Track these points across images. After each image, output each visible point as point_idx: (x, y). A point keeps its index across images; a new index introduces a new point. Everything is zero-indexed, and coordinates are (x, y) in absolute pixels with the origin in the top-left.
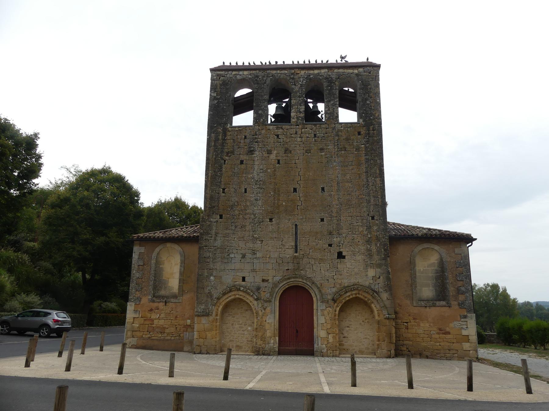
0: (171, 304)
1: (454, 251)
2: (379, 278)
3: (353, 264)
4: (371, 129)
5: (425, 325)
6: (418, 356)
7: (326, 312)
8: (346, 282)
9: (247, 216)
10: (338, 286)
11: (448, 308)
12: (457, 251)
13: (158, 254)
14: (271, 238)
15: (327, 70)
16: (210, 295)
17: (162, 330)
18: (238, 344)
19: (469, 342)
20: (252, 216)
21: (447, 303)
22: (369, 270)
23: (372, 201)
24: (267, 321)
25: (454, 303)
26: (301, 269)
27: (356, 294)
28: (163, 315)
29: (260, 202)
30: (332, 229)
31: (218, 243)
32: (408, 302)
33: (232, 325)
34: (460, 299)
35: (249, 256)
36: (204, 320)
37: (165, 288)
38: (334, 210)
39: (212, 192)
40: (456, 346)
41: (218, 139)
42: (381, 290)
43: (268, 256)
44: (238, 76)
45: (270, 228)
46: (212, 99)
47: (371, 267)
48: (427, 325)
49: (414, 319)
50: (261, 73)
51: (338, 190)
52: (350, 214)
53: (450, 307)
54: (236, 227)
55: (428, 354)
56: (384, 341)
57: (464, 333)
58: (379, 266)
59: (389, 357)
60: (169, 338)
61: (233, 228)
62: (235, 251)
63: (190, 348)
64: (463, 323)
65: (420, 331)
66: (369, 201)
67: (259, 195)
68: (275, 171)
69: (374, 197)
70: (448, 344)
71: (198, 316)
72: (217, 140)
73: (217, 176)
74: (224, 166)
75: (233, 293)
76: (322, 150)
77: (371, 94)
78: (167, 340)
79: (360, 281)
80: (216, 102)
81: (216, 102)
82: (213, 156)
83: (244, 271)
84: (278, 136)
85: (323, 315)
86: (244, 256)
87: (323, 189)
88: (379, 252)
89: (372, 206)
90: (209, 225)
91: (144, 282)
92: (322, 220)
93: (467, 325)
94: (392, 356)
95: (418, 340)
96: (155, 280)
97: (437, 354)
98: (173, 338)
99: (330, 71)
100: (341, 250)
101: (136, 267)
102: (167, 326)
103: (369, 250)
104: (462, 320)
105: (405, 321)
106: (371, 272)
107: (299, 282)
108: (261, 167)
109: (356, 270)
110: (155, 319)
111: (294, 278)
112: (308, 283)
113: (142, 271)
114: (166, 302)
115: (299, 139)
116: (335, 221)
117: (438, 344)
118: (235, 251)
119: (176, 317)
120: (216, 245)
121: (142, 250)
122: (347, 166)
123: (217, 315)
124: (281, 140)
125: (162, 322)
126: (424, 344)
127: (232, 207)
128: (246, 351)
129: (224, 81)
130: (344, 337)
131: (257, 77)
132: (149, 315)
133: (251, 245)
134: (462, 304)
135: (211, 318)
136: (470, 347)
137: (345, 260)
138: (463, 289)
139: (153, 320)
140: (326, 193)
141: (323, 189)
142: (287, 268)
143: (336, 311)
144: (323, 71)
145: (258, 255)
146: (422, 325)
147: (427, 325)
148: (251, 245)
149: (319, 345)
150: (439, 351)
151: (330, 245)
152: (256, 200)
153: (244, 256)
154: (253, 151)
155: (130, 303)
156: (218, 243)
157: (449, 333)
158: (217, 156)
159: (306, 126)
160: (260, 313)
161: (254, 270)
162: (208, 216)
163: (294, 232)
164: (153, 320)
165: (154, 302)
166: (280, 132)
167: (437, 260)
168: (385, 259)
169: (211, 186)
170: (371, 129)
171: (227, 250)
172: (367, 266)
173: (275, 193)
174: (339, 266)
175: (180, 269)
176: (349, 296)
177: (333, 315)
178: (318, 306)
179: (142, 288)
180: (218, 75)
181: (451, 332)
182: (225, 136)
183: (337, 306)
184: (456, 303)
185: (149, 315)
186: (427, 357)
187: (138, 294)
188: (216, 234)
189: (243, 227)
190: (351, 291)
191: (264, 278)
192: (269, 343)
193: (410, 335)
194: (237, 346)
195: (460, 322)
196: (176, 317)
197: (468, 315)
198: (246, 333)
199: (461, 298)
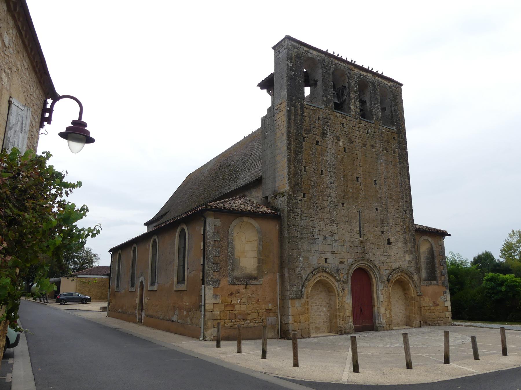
0: (251, 286)
7: (383, 291)
8: (394, 266)
9: (325, 198)
14: (344, 222)
15: (324, 55)
16: (300, 276)
17: (244, 316)
18: (317, 325)
20: (329, 199)
24: (346, 302)
28: (244, 300)
29: (334, 186)
31: (304, 223)
35: (329, 238)
36: (297, 303)
37: (238, 268)
38: (384, 202)
39: (295, 168)
40: (442, 315)
41: (297, 114)
42: (414, 272)
44: (309, 53)
45: (343, 212)
50: (326, 58)
54: (317, 208)
55: (429, 322)
60: (252, 325)
62: (318, 232)
63: (273, 334)
66: (403, 199)
67: (333, 179)
68: (343, 158)
69: (405, 194)
71: (292, 299)
73: (298, 152)
74: (304, 143)
75: (319, 275)
78: (251, 327)
79: (402, 264)
80: (293, 73)
81: (293, 73)
82: (294, 130)
85: (382, 294)
86: (325, 238)
90: (295, 203)
91: (221, 261)
92: (377, 209)
97: (434, 321)
98: (256, 325)
100: (389, 237)
101: (212, 242)
102: (249, 312)
103: (405, 239)
108: (333, 152)
110: (237, 304)
111: (362, 260)
112: (371, 266)
113: (218, 247)
114: (246, 285)
115: (358, 132)
118: (318, 232)
119: (258, 301)
120: (301, 224)
121: (218, 222)
124: (346, 130)
125: (243, 308)
126: (427, 315)
127: (313, 186)
128: (323, 332)
131: (324, 61)
132: (229, 300)
133: (330, 227)
139: (234, 306)
145: (336, 237)
148: (330, 227)
149: (381, 321)
151: (383, 232)
152: (331, 183)
153: (325, 238)
154: (326, 134)
155: (208, 286)
157: (438, 305)
158: (297, 130)
159: (362, 122)
160: (341, 294)
161: (333, 252)
162: (294, 193)
164: (234, 306)
165: (234, 284)
166: (344, 121)
167: (427, 249)
168: (414, 247)
169: (294, 162)
171: (311, 230)
173: (344, 179)
174: (389, 251)
175: (258, 248)
179: (220, 268)
180: (293, 46)
185: (229, 300)
186: (429, 325)
187: (216, 275)
188: (302, 212)
189: (323, 208)
191: (341, 260)
192: (348, 323)
194: (316, 328)
196: (258, 301)
198: (322, 314)
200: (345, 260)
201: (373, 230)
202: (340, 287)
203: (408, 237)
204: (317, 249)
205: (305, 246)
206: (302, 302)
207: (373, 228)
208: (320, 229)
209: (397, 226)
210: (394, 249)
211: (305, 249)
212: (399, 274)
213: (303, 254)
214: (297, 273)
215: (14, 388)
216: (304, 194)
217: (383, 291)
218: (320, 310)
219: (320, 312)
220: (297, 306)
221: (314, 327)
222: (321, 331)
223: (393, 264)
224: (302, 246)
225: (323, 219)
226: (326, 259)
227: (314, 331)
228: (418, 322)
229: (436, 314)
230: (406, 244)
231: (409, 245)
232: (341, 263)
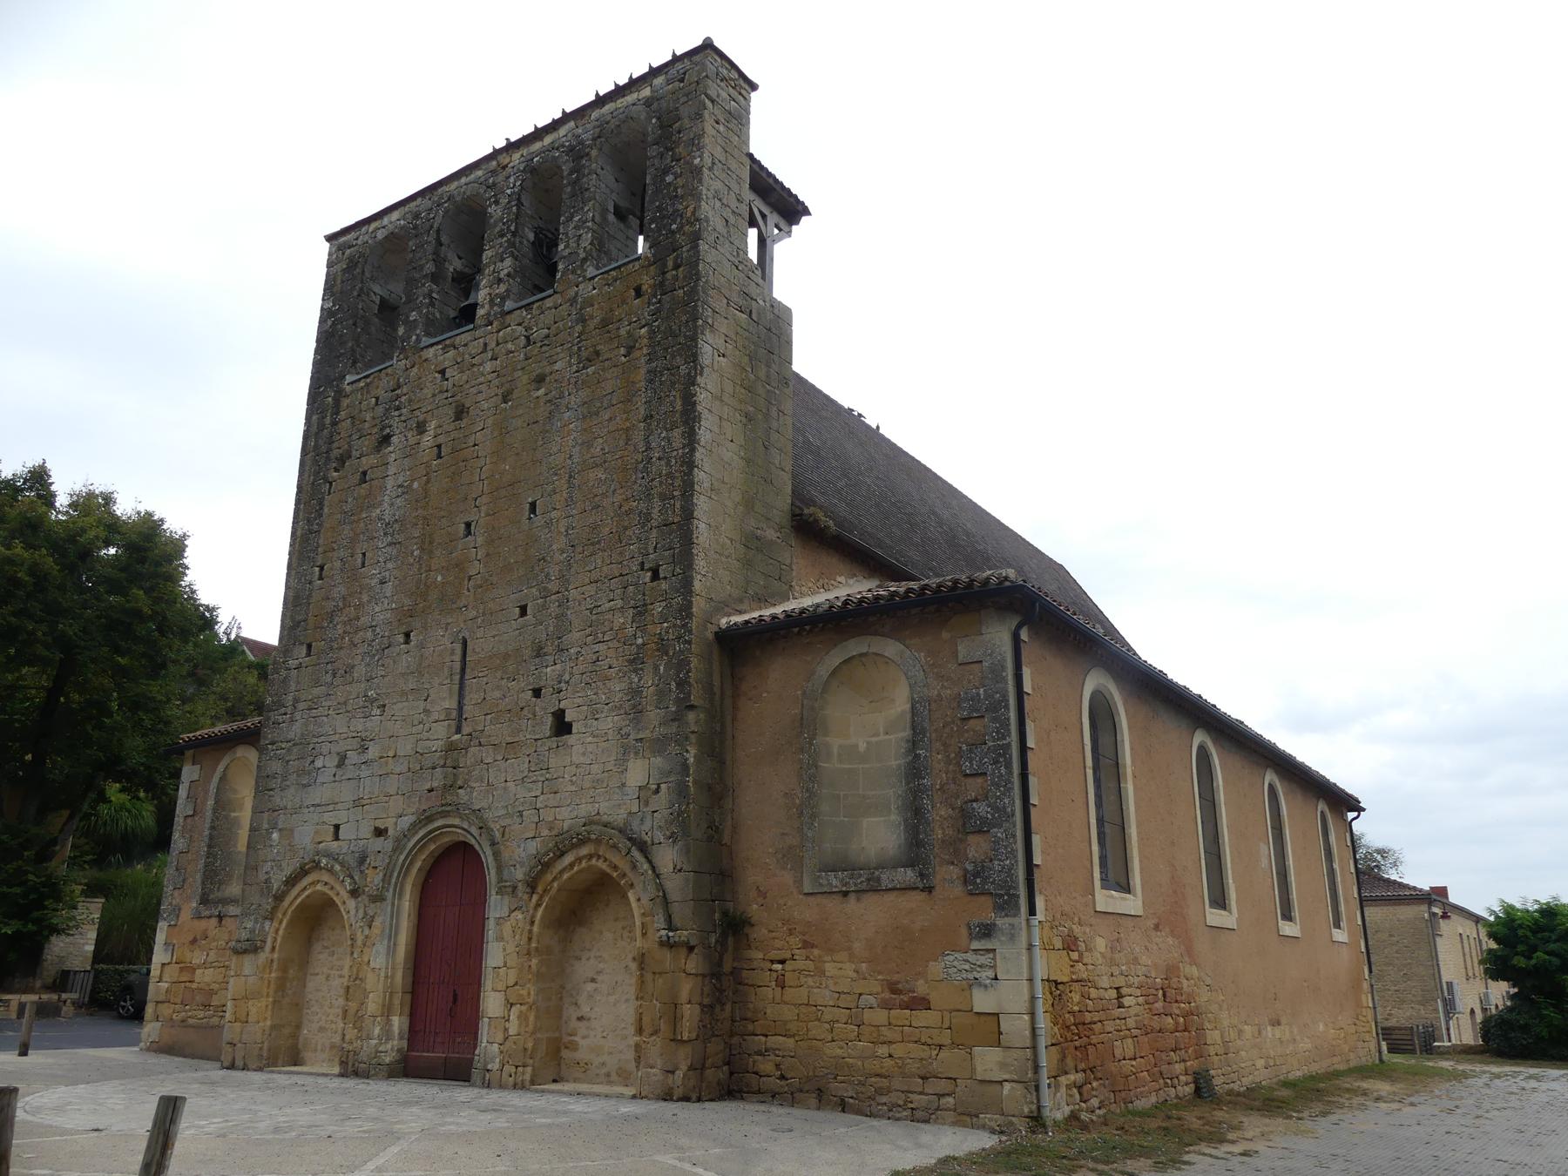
1: (955, 654)
2: (657, 791)
3: (590, 748)
4: (670, 264)
5: (841, 971)
6: (813, 1101)
7: (507, 928)
8: (568, 816)
10: (545, 832)
11: (924, 894)
12: (964, 650)
13: (223, 779)
14: (404, 693)
19: (999, 1045)
21: (922, 875)
22: (630, 764)
23: (655, 513)
24: (372, 964)
25: (947, 875)
26: (460, 783)
27: (590, 857)
30: (544, 636)
31: (295, 731)
32: (787, 878)
33: (327, 978)
34: (972, 853)
35: (353, 757)
38: (554, 571)
40: (948, 1060)
43: (391, 754)
46: (326, 314)
47: (636, 753)
48: (849, 970)
49: (807, 945)
51: (570, 501)
52: (594, 576)
53: (929, 890)
55: (848, 1092)
56: (655, 1033)
57: (983, 1001)
58: (659, 745)
59: (667, 1096)
61: (329, 678)
64: (982, 959)
65: (824, 996)
68: (428, 482)
69: (663, 497)
70: (918, 1051)
72: (321, 427)
76: (540, 380)
77: (680, 150)
79: (604, 807)
83: (339, 806)
84: (443, 372)
87: (533, 506)
88: (661, 694)
89: (654, 533)
92: (523, 611)
93: (994, 967)
94: (678, 1093)
95: (813, 1033)
96: (209, 855)
97: (880, 1091)
99: (580, 123)
104: (975, 945)
105: (774, 955)
106: (637, 773)
107: (458, 828)
109: (595, 768)
110: (199, 967)
114: (220, 917)
116: (554, 608)
117: (882, 1050)
122: (597, 414)
123: (273, 948)
129: (351, 259)
130: (580, 1019)
134: (976, 874)
135: (263, 956)
136: (1003, 1066)
137: (570, 739)
138: (982, 809)
140: (539, 520)
141: (533, 506)
142: (428, 786)
143: (532, 923)
144: (562, 131)
145: (373, 752)
146: (830, 968)
147: (849, 970)
149: (489, 1046)
150: (884, 1083)
151: (537, 693)
156: (295, 731)
157: (923, 1004)
160: (360, 938)
161: (358, 803)
163: (457, 666)
170: (670, 264)
172: (626, 750)
174: (553, 762)
176: (572, 865)
177: (525, 939)
178: (496, 906)
181: (934, 998)
182: (337, 413)
183: (538, 905)
184: (954, 872)
186: (843, 1107)
188: (296, 700)
189: (349, 669)
190: (574, 846)
193: (788, 1013)
195: (971, 957)
197: (999, 922)
199: (976, 847)
200: (389, 823)
201: (497, 694)
203: (649, 680)
204: (317, 801)
207: (498, 687)
208: (332, 738)
209: (602, 647)
212: (584, 851)
214: (262, 877)
215: (81, 1104)
216: (309, 646)
217: (507, 928)
220: (246, 972)
223: (564, 813)
226: (337, 827)
229: (898, 1050)
231: (654, 715)
232: (380, 832)
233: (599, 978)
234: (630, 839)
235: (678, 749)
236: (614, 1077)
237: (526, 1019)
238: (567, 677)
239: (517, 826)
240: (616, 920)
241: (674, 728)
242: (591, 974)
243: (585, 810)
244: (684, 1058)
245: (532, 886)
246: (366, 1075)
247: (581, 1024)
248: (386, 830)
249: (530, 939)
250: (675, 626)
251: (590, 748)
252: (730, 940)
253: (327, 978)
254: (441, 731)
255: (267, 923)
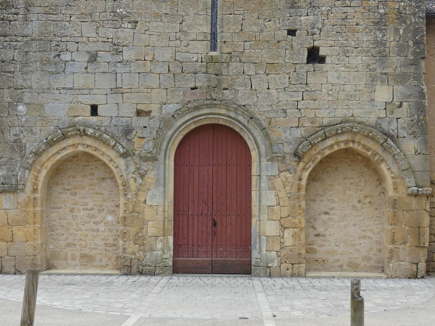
2: (400, 106)
7: (278, 182)
8: (325, 116)
14: (157, 16)
18: (87, 251)
22: (378, 88)
24: (149, 203)
26: (225, 86)
31: (33, 28)
35: (105, 57)
42: (403, 133)
56: (405, 243)
58: (402, 79)
62: (72, 47)
79: (357, 112)
86: (93, 58)
100: (316, 44)
103: (380, 44)
106: (383, 94)
107: (221, 115)
109: (348, 88)
111: (208, 106)
112: (240, 118)
118: (72, 47)
120: (27, 31)
123: (35, 190)
130: (318, 235)
142: (192, 85)
143: (300, 179)
151: (292, 33)
153: (93, 58)
156: (33, 28)
160: (133, 186)
161: (117, 90)
171: (54, 44)
172: (373, 79)
174: (311, 80)
178: (261, 168)
183: (304, 169)
191: (140, 107)
192: (151, 250)
194: (83, 256)
198: (102, 227)
201: (255, 28)
202: (132, 168)
205: (35, 80)
206: (20, 200)
208: (79, 40)
210: (330, 74)
211: (35, 86)
212: (344, 138)
213: (27, 98)
218: (98, 219)
219: (96, 223)
220: (6, 206)
221: (78, 254)
222: (95, 264)
224: (25, 80)
225: (91, 15)
227: (77, 262)
228: (406, 265)
230: (383, 56)
233: (332, 212)
234: (385, 134)
235: (415, 83)
236: (345, 267)
237: (299, 237)
238: (320, 26)
239: (282, 119)
240: (345, 179)
241: (412, 69)
242: (326, 210)
243: (341, 113)
244: (423, 255)
245: (298, 156)
246: (152, 274)
247: (317, 238)
248: (150, 112)
249: (299, 189)
250: (410, 6)
251: (343, 74)
252: (41, 150)
253: (72, 210)
254: (202, 48)
255: (27, 172)
